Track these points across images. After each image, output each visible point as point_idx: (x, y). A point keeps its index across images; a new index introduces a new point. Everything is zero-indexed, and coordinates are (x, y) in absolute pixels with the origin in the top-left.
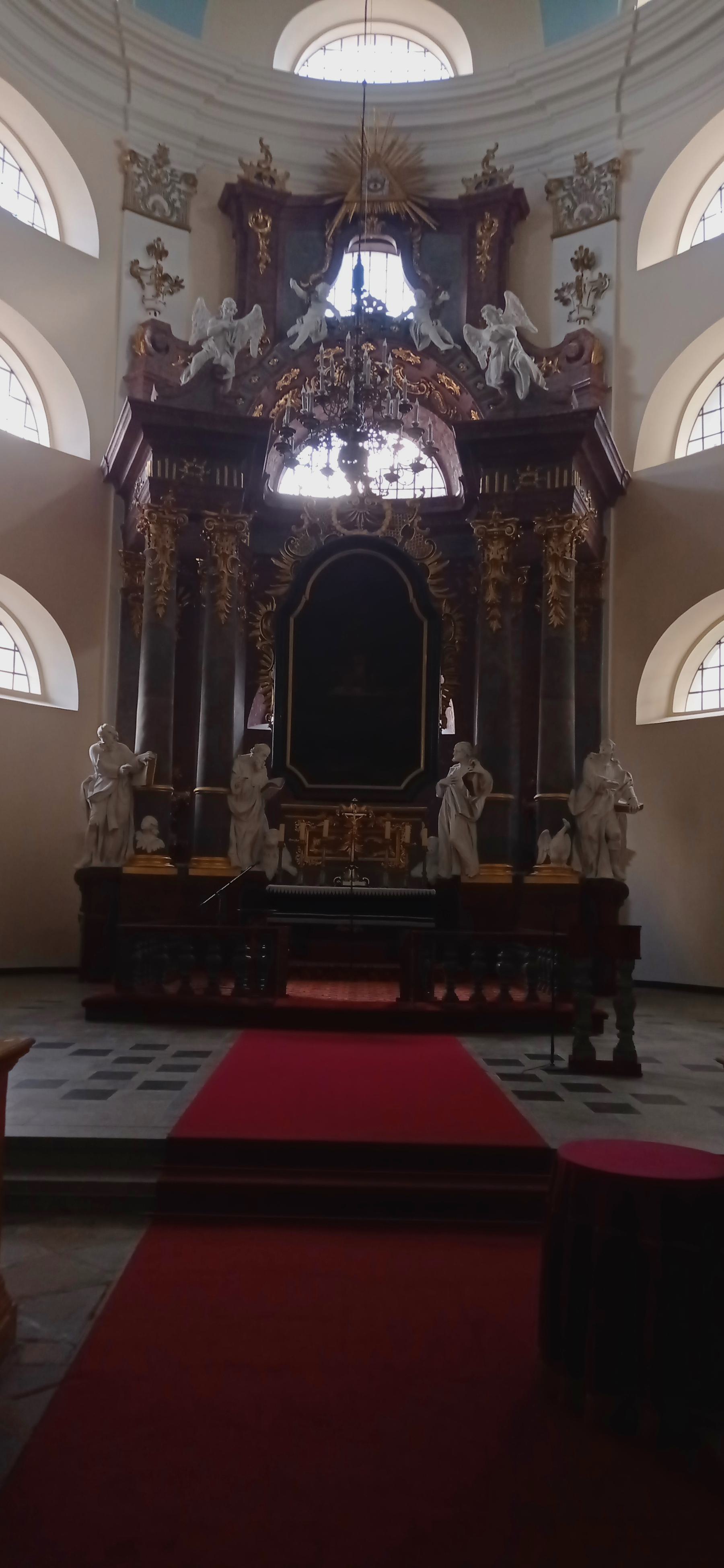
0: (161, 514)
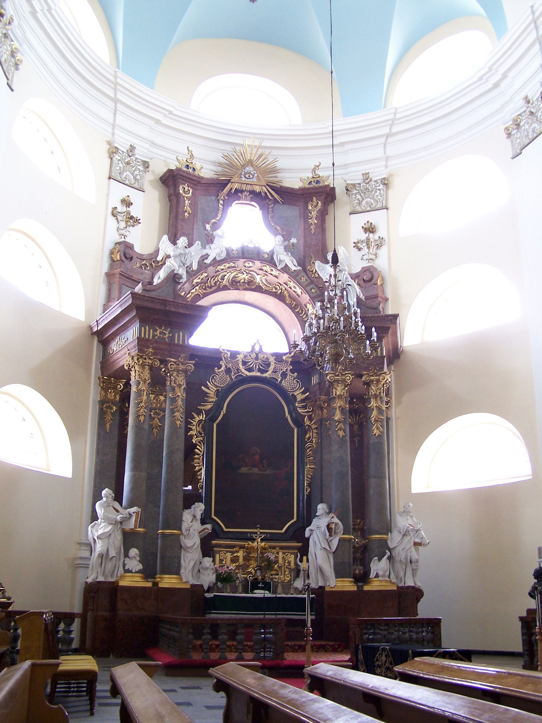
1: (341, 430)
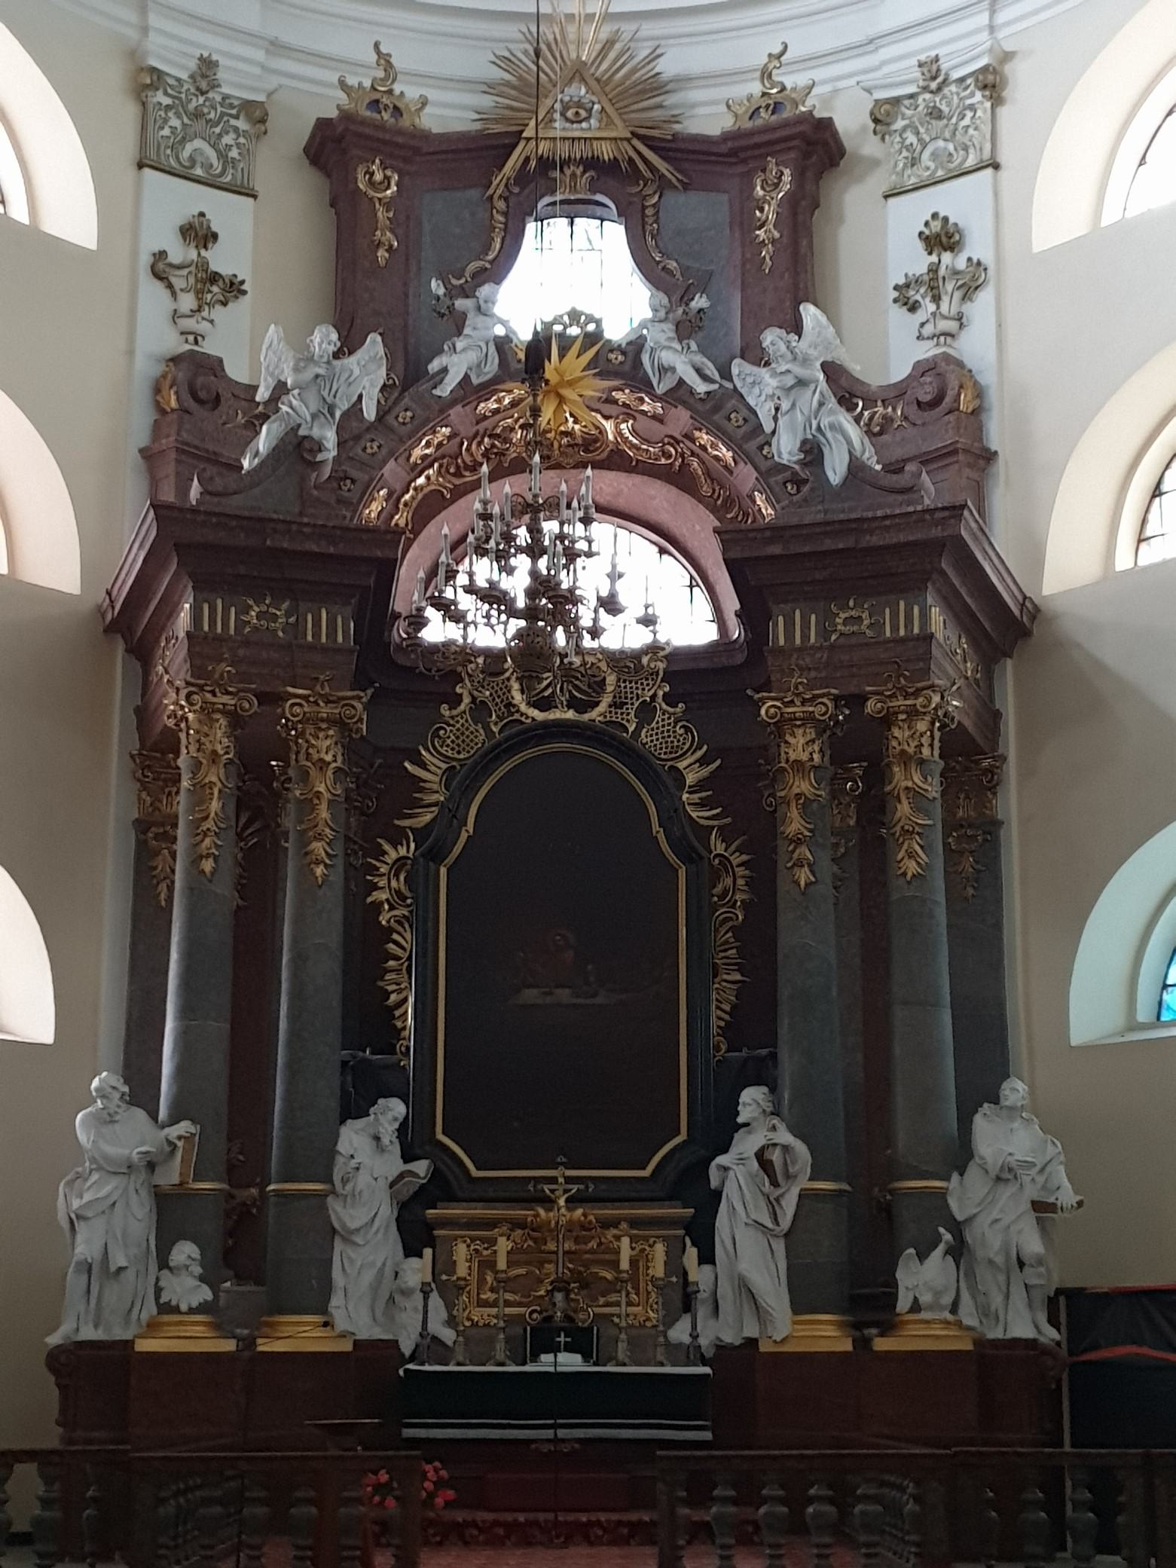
0: (209, 696)
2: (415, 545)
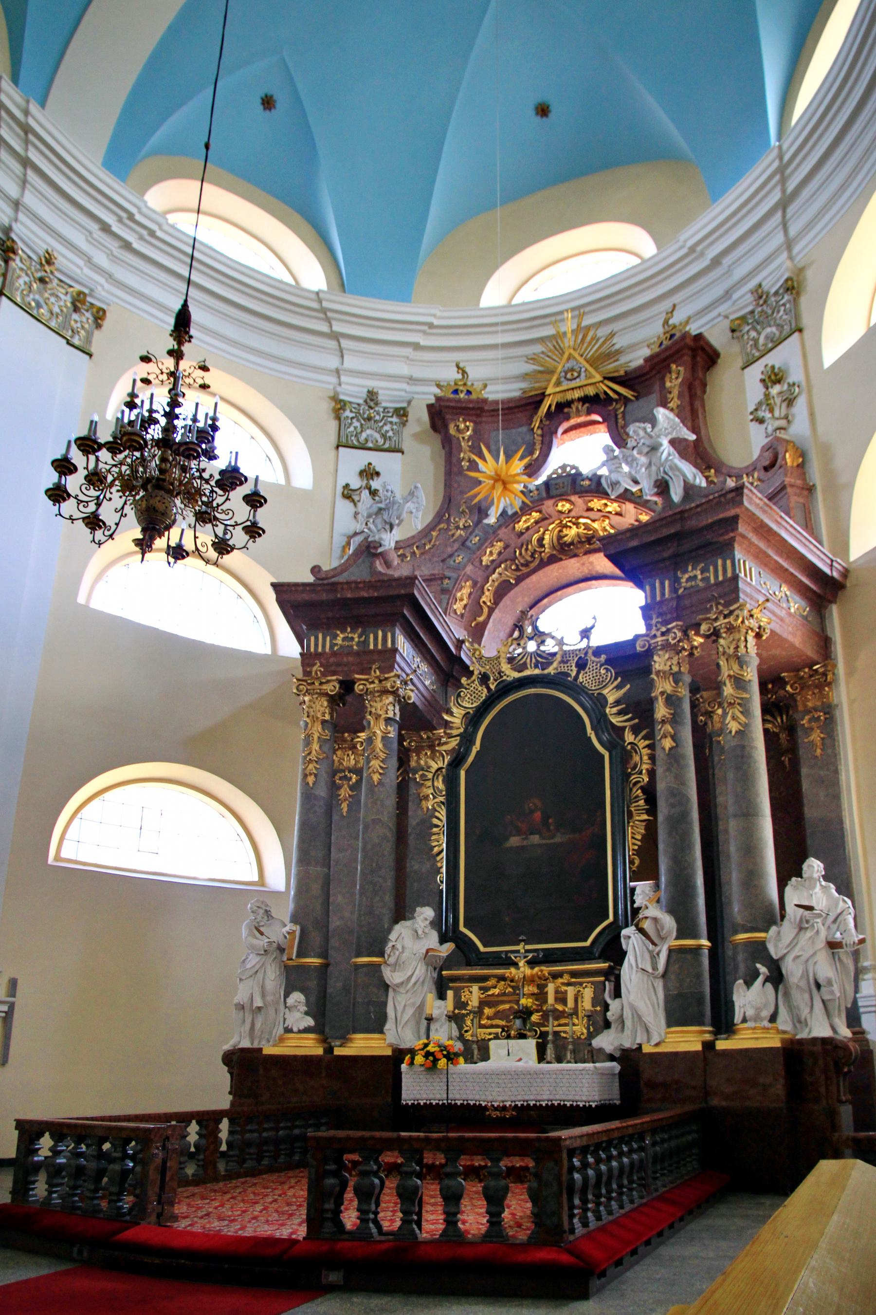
1: (666, 737)
2: (497, 611)
